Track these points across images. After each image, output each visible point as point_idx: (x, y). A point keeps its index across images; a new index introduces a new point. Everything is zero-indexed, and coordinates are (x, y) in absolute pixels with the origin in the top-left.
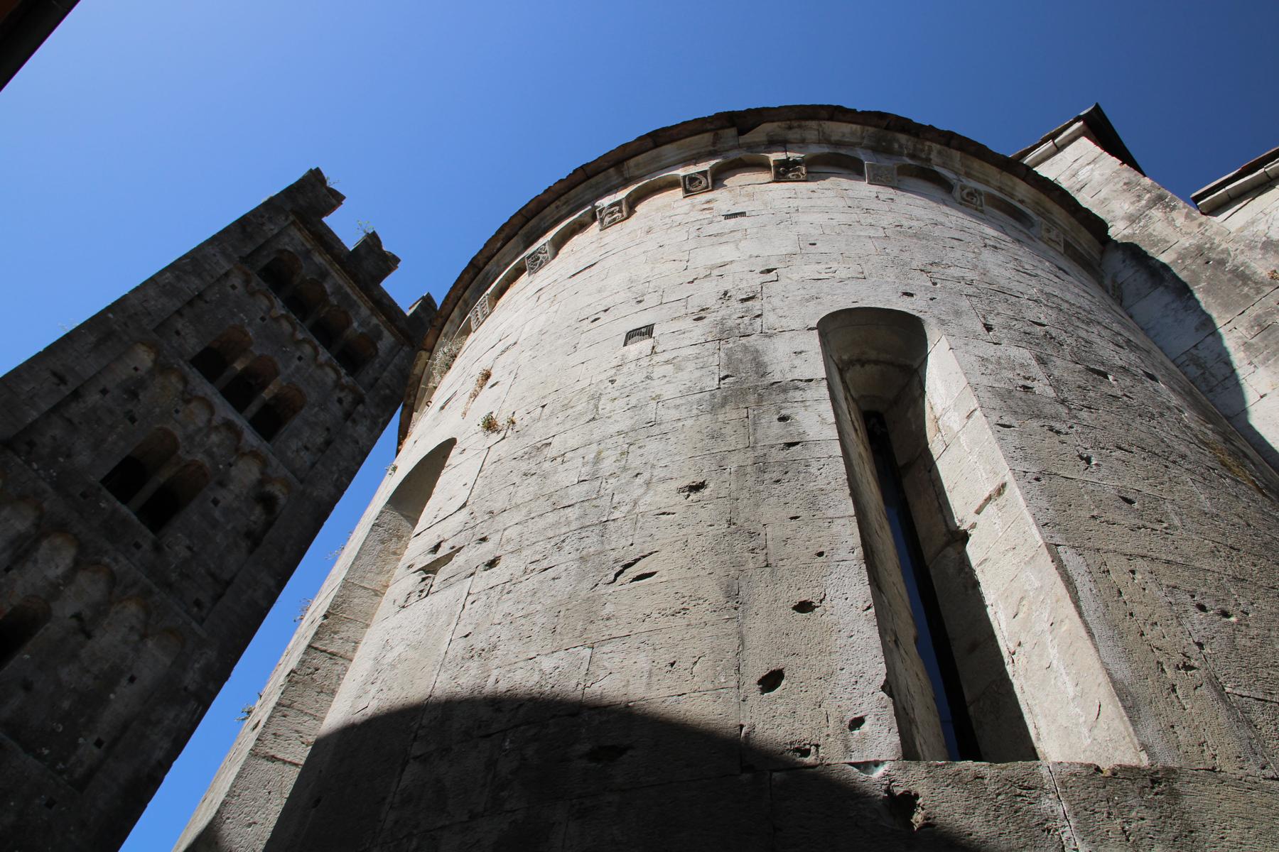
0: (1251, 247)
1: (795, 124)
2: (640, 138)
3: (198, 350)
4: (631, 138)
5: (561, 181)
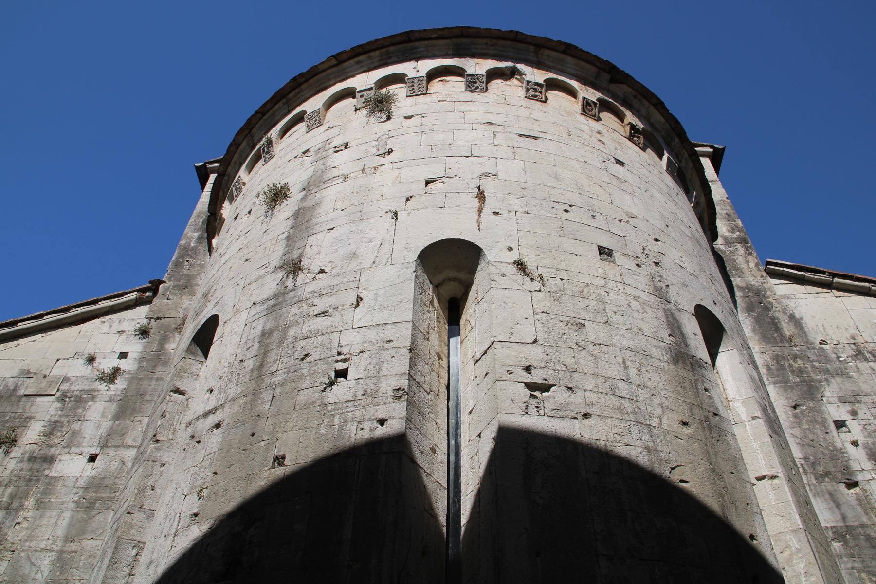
0: (785, 313)
1: (639, 97)
2: (560, 42)
4: (555, 38)
5: (500, 30)
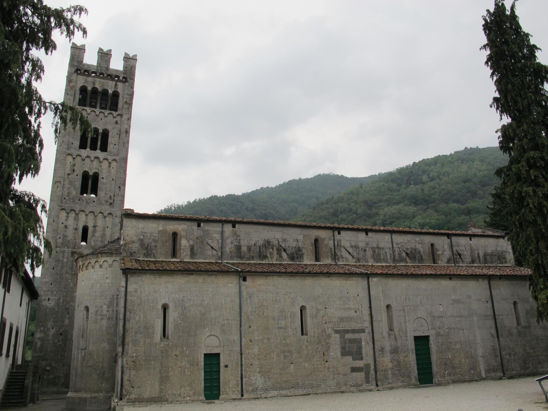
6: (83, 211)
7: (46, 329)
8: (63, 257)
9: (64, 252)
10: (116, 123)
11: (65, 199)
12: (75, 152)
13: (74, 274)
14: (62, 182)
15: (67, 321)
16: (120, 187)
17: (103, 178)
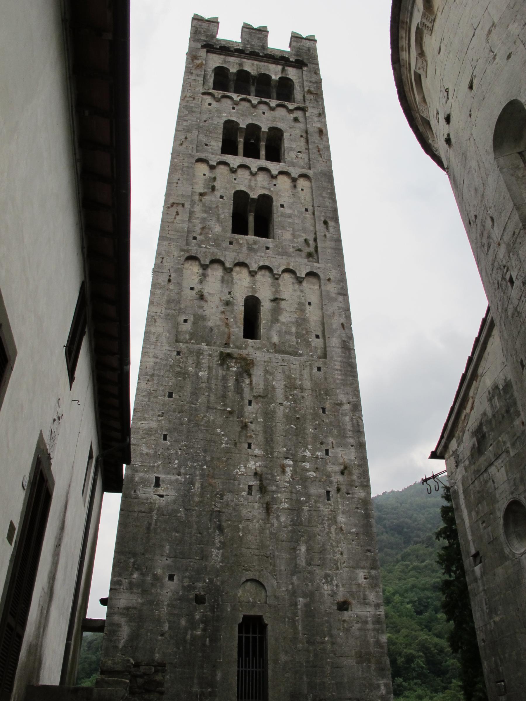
3: (220, 144)
6: (242, 264)
7: (149, 578)
8: (198, 365)
9: (199, 353)
10: (296, 120)
11: (195, 238)
12: (213, 160)
13: (230, 413)
14: (187, 206)
15: (216, 555)
16: (325, 223)
17: (282, 206)
